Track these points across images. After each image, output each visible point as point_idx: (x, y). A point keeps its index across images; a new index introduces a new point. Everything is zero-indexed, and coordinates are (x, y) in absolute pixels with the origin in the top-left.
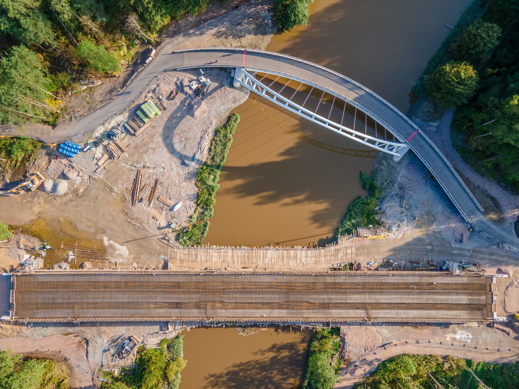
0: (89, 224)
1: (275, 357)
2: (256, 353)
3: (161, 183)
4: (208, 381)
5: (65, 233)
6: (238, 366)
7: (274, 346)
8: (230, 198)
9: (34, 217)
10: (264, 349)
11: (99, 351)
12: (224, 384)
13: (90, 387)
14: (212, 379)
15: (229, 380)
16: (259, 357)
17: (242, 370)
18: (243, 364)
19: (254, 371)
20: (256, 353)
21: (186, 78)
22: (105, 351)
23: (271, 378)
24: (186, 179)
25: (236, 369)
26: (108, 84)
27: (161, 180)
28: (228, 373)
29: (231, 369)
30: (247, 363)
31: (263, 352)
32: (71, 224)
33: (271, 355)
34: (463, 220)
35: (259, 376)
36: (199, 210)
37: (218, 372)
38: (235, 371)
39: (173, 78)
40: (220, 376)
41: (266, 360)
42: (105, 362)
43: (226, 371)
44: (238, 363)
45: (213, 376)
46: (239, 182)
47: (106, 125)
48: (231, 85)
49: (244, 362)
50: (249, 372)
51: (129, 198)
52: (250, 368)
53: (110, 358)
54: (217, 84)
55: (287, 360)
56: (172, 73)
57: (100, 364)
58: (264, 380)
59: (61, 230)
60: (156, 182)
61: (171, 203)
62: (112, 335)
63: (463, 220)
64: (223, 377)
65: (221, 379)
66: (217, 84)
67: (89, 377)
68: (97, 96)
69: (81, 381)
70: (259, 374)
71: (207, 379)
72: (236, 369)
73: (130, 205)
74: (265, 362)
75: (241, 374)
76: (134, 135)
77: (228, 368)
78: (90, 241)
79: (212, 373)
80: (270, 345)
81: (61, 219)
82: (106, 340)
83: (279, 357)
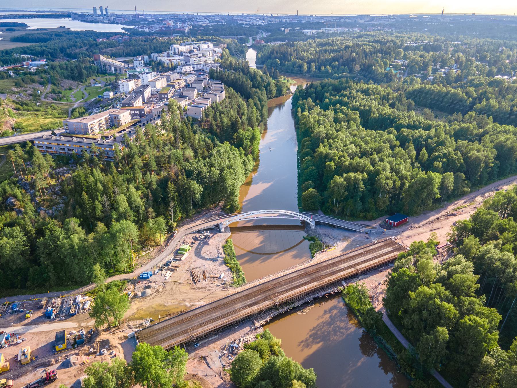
0: (173, 301)
1: (330, 317)
2: (318, 319)
3: (207, 271)
4: (301, 346)
5: (159, 311)
6: (313, 330)
7: (325, 312)
8: (247, 265)
9: (135, 311)
10: (321, 315)
11: (216, 360)
12: (313, 343)
13: (222, 384)
14: (303, 344)
15: (314, 339)
16: (321, 320)
17: (318, 331)
18: (316, 328)
19: (325, 328)
20: (318, 319)
21: (197, 235)
22: (220, 357)
23: (339, 327)
24: (220, 266)
25: (313, 331)
26: (157, 249)
27: (205, 270)
28: (310, 336)
29: (310, 333)
30: (318, 325)
31: (322, 317)
32: (161, 305)
33: (328, 316)
34: (360, 233)
35: (331, 329)
36: (235, 274)
37: (304, 338)
38: (314, 333)
39: (191, 236)
40: (307, 340)
41: (327, 319)
42: (224, 363)
43: (308, 336)
44: (312, 328)
45: (302, 342)
46: (246, 259)
47: (163, 261)
48: (220, 232)
49: (315, 326)
50: (323, 330)
51: (192, 282)
52: (322, 327)
53: (227, 359)
54: (141, 97)
55: (339, 314)
56: (190, 235)
57: (222, 366)
58: (336, 329)
59: (156, 310)
60: (204, 272)
61: (218, 276)
62: (219, 347)
63: (360, 233)
64: (309, 339)
65: (308, 341)
66: (141, 97)
67: (218, 378)
68: (153, 254)
69: (213, 384)
70: (330, 327)
71: (299, 345)
72: (313, 331)
73: (194, 285)
74: (328, 321)
75: (319, 333)
76: (181, 260)
77: (308, 333)
78: (178, 308)
79: (300, 341)
80: (323, 312)
81: (153, 306)
82: (217, 351)
83: (334, 315)
